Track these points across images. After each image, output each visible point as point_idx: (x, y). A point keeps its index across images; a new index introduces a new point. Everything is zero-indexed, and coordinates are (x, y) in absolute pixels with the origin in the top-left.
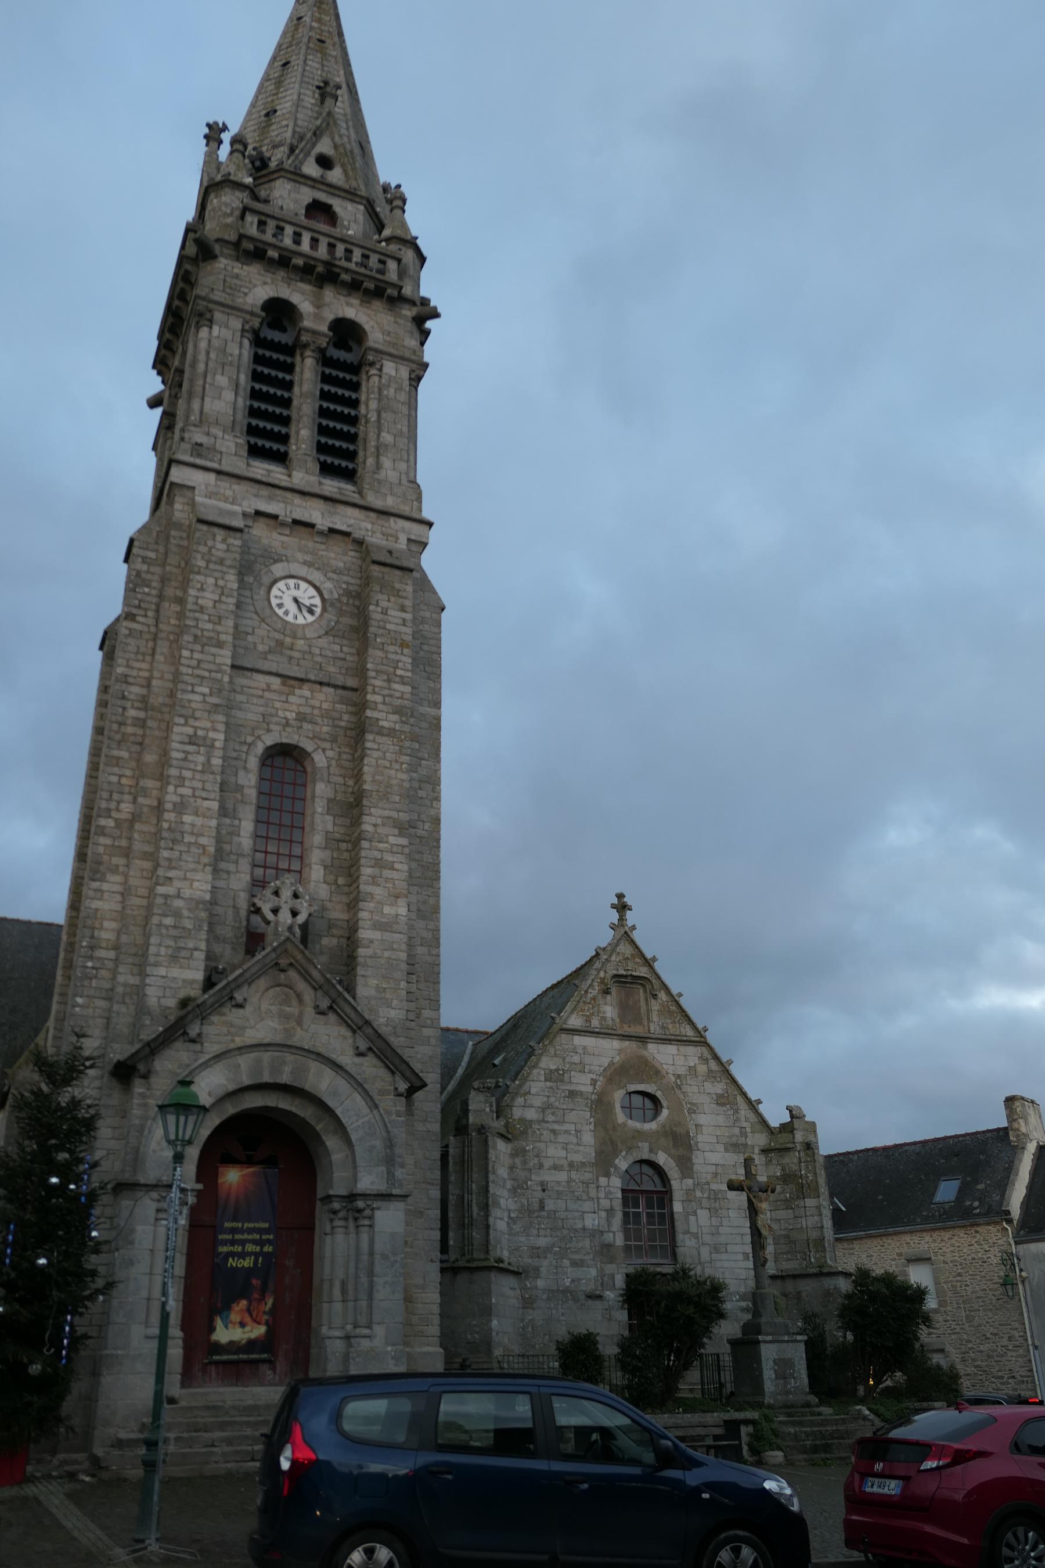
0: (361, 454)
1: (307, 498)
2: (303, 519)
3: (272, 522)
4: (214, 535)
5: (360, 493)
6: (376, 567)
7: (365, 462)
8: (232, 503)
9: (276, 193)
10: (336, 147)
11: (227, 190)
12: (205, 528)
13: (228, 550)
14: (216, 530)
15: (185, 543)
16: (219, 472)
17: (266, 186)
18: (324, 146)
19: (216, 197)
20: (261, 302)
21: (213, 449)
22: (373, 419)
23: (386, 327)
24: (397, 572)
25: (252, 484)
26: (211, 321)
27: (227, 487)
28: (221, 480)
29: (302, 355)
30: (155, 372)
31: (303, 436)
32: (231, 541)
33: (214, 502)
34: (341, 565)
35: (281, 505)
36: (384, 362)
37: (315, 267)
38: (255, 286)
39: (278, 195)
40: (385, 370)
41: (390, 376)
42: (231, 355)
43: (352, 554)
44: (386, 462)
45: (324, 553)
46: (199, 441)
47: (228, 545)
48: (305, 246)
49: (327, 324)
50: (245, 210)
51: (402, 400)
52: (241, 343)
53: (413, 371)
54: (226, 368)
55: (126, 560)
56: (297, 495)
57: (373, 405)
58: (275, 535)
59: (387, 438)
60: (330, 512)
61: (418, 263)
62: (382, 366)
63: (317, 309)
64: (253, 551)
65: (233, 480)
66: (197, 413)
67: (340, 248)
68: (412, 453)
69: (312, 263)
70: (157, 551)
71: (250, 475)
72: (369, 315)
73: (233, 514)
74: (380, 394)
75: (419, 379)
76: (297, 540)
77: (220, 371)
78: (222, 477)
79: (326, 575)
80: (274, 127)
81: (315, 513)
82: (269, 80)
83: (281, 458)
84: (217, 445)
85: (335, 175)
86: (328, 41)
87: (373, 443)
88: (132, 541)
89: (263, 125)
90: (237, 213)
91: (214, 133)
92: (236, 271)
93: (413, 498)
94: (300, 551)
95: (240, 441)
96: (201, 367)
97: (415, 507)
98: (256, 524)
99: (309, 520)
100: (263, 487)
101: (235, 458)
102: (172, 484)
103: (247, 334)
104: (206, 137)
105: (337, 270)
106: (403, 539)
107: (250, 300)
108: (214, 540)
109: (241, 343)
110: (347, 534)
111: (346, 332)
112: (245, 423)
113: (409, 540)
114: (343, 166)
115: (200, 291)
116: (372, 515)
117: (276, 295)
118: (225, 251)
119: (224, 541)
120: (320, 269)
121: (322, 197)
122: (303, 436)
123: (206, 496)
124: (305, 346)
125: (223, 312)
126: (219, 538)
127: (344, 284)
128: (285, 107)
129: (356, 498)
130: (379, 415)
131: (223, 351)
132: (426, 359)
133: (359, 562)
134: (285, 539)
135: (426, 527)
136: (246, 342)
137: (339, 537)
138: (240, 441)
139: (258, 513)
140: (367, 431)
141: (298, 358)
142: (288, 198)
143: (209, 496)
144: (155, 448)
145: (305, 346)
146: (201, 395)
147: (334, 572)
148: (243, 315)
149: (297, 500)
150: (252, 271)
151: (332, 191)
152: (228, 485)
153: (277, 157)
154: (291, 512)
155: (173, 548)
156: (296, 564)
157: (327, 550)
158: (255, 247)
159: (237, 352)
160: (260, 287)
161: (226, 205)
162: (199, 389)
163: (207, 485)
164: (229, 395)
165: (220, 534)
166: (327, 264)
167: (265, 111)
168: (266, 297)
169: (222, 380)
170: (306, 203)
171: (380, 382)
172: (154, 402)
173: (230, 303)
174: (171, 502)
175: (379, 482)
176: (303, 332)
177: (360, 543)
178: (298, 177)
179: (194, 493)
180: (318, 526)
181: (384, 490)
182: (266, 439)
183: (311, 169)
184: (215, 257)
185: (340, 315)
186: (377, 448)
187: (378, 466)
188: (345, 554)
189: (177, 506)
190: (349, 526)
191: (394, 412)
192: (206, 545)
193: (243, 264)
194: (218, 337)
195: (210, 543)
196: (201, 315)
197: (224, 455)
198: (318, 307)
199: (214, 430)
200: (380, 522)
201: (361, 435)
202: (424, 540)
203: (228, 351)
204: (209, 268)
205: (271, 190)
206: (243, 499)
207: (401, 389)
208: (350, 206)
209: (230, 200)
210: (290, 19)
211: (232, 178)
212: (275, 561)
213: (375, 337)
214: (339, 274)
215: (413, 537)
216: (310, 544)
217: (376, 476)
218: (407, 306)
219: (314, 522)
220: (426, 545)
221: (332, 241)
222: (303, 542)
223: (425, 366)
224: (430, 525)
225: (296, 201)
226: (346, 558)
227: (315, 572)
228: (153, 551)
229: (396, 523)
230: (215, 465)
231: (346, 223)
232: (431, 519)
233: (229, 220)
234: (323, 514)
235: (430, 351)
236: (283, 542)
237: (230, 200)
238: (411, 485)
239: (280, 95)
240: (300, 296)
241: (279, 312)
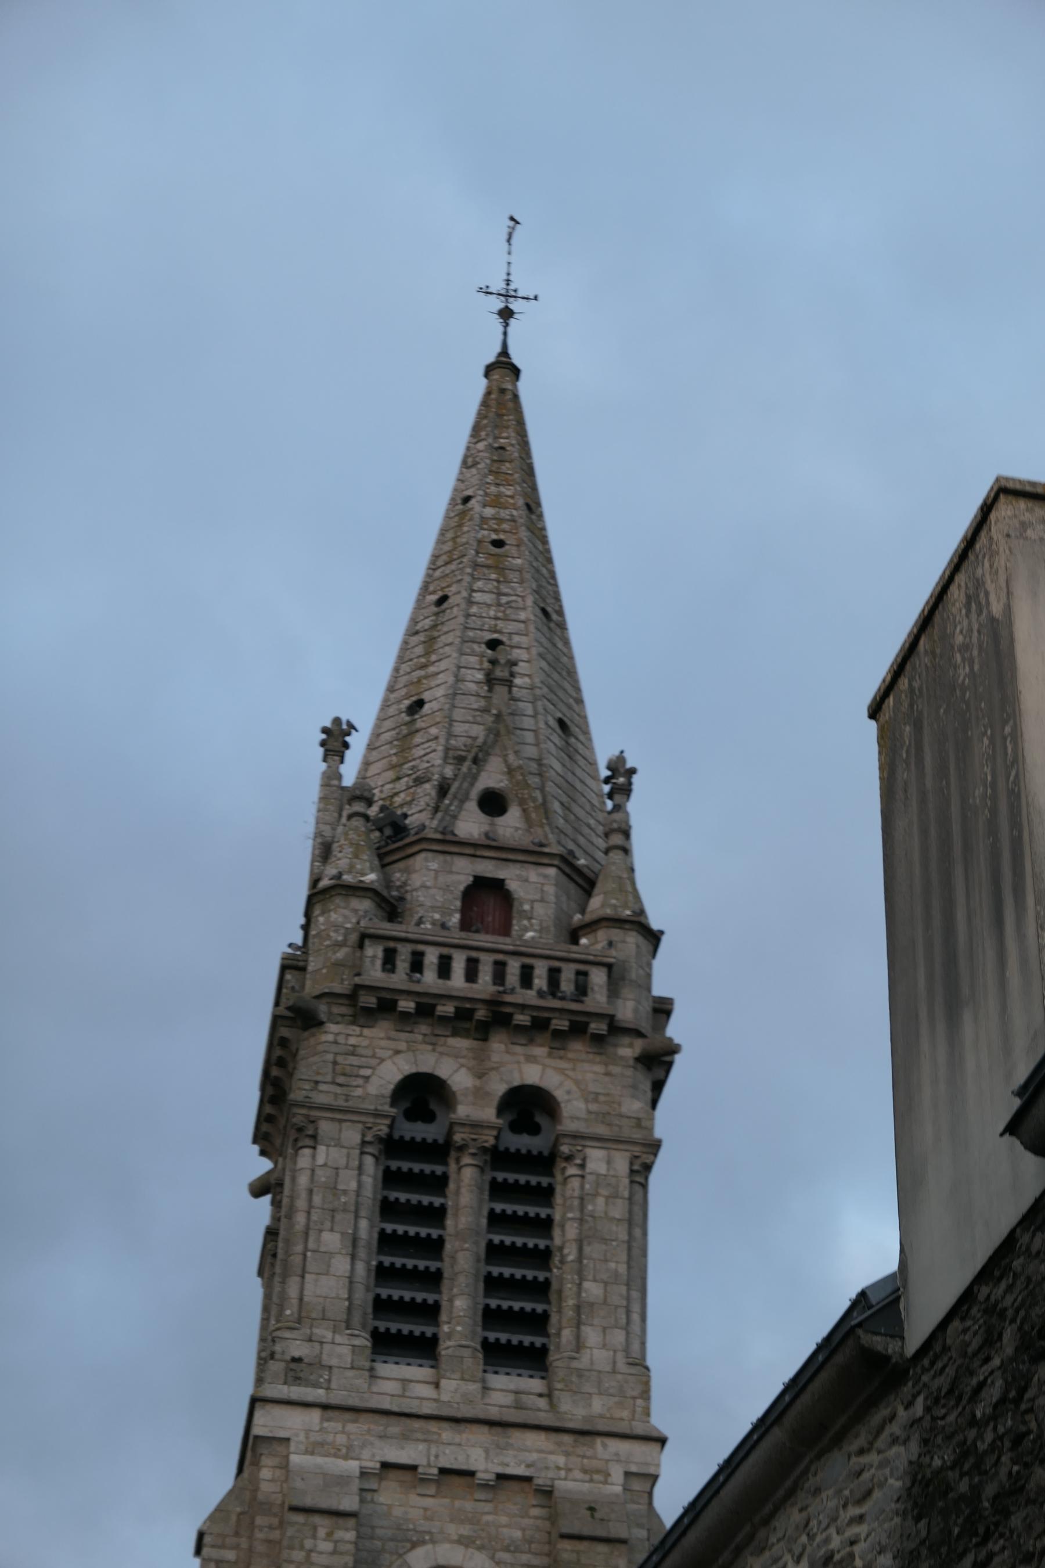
0: (554, 1319)
1: (462, 1427)
2: (455, 1466)
3: (407, 1476)
4: (315, 1528)
5: (548, 1395)
6: (567, 1545)
7: (558, 1334)
8: (346, 1458)
9: (416, 880)
10: (510, 771)
11: (338, 900)
12: (300, 1518)
13: (335, 1552)
14: (317, 1519)
15: (276, 1535)
16: (325, 1407)
17: (401, 865)
18: (493, 776)
19: (323, 913)
20: (392, 1087)
21: (318, 1364)
22: (571, 1258)
23: (592, 1088)
24: (602, 1548)
25: (377, 1417)
26: (314, 1137)
27: (339, 1430)
28: (328, 1420)
29: (458, 1160)
30: (256, 1148)
31: (460, 1307)
32: (340, 1534)
33: (319, 1460)
34: (518, 1534)
35: (421, 1447)
36: (589, 1152)
37: (472, 1011)
38: (382, 1060)
39: (418, 884)
40: (591, 1166)
41: (598, 1175)
42: (345, 1192)
43: (535, 1512)
44: (591, 1335)
45: (490, 1518)
46: (297, 1354)
47: (336, 1542)
48: (458, 980)
49: (495, 1102)
50: (364, 938)
51: (618, 1216)
52: (360, 1168)
53: (637, 1157)
54: (339, 1217)
55: (198, 1552)
56: (445, 1425)
57: (572, 1231)
58: (414, 1499)
59: (593, 1290)
60: (498, 1447)
61: (645, 945)
62: (584, 1159)
63: (476, 1080)
64: (379, 1532)
65: (348, 1416)
66: (295, 1302)
67: (514, 967)
68: (636, 1308)
69: (468, 1006)
70: (236, 1547)
71: (374, 1403)
72: (561, 1071)
73: (342, 1480)
74: (582, 1208)
75: (648, 1168)
76: (447, 1501)
77: (328, 1224)
78: (330, 1414)
79: (492, 1558)
80: (418, 739)
81: (476, 1452)
82: (417, 633)
83: (425, 1349)
84: (324, 1357)
85: (510, 825)
86: (510, 540)
87: (571, 1302)
88: (201, 1535)
89: (405, 730)
90: (354, 937)
91: (335, 740)
92: (352, 1041)
93: (635, 1393)
94: (452, 1521)
95: (357, 1342)
96: (300, 1219)
97: (639, 1410)
98: (384, 1484)
99: (464, 1467)
100: (393, 1420)
101: (350, 1373)
102: (256, 1437)
103: (369, 1149)
104: (323, 744)
105: (508, 1010)
106: (617, 1474)
107: (372, 1089)
108: (314, 1537)
109: (360, 1168)
110: (528, 1479)
111: (527, 1106)
112: (370, 1297)
113: (628, 1474)
114: (522, 802)
115: (296, 1095)
116: (567, 1439)
117: (414, 1070)
118: (336, 1010)
119: (330, 1535)
120: (481, 1014)
121: (488, 869)
122: (460, 1307)
123: (307, 1452)
124: (461, 1149)
125: (332, 1119)
126: (322, 1532)
127: (520, 1029)
128: (436, 697)
129: (540, 1411)
130: (580, 1250)
131: (333, 1188)
132: (658, 1133)
133: (547, 1524)
134: (429, 1502)
135: (656, 1446)
136: (369, 1161)
137: (514, 1485)
138: (357, 1342)
139: (386, 1466)
140: (562, 1275)
141: (453, 1166)
142: (434, 886)
143: (311, 1450)
144: (260, 1273)
145: (461, 1149)
146: (299, 1272)
147: (507, 1549)
148: (363, 1119)
149: (447, 1433)
150: (378, 1036)
151: (504, 855)
152: (339, 1426)
153: (417, 817)
154: (437, 1456)
155: (260, 1548)
156: (447, 1546)
157: (495, 1513)
158: (379, 999)
159: (353, 1185)
160: (388, 1060)
161: (337, 927)
162: (297, 1260)
163: (308, 1432)
164: (341, 1265)
165: (323, 1524)
166: (493, 1004)
167: (408, 706)
168: (399, 1077)
169: (331, 1240)
170: (462, 888)
171: (582, 1187)
172: (259, 1189)
173: (341, 1102)
174: (256, 1463)
175: (580, 1373)
176: (456, 1128)
177: (547, 1493)
178: (449, 844)
179: (288, 1447)
180: (479, 1475)
181: (588, 1388)
182: (401, 1327)
183: (471, 824)
184: (321, 1023)
185: (516, 1083)
186: (578, 1308)
187: (579, 1345)
188: (525, 1515)
189: (265, 1474)
190: (528, 1466)
191: (605, 1241)
192: (302, 1547)
193: (362, 1026)
194: (325, 1165)
195: (308, 1543)
196: (300, 1130)
197: (335, 1371)
198: (480, 1076)
199: (323, 1332)
200: (580, 1451)
201: (555, 1286)
202: (652, 1470)
203: (341, 1187)
204: (312, 1041)
205: (408, 871)
206: (363, 1446)
207: (615, 1196)
208: (533, 874)
209: (346, 916)
210: (453, 502)
211: (347, 878)
212: (414, 1545)
213: (574, 1110)
214: (511, 1015)
215: (634, 1469)
216: (469, 1506)
217: (575, 1364)
218: (626, 1040)
219: (473, 1468)
220: (655, 1478)
221: (500, 957)
222: (458, 1504)
223: (655, 1146)
224: (662, 1441)
225: (446, 889)
226: (527, 1522)
227: (477, 1553)
228: (232, 1548)
229: (604, 1446)
230: (318, 1394)
231: (527, 907)
232: (665, 1429)
233: (341, 954)
234: (487, 1451)
235: (665, 1121)
236: (426, 1509)
237: (346, 916)
238: (633, 1370)
239: (432, 669)
240: (452, 1064)
241: (421, 1094)
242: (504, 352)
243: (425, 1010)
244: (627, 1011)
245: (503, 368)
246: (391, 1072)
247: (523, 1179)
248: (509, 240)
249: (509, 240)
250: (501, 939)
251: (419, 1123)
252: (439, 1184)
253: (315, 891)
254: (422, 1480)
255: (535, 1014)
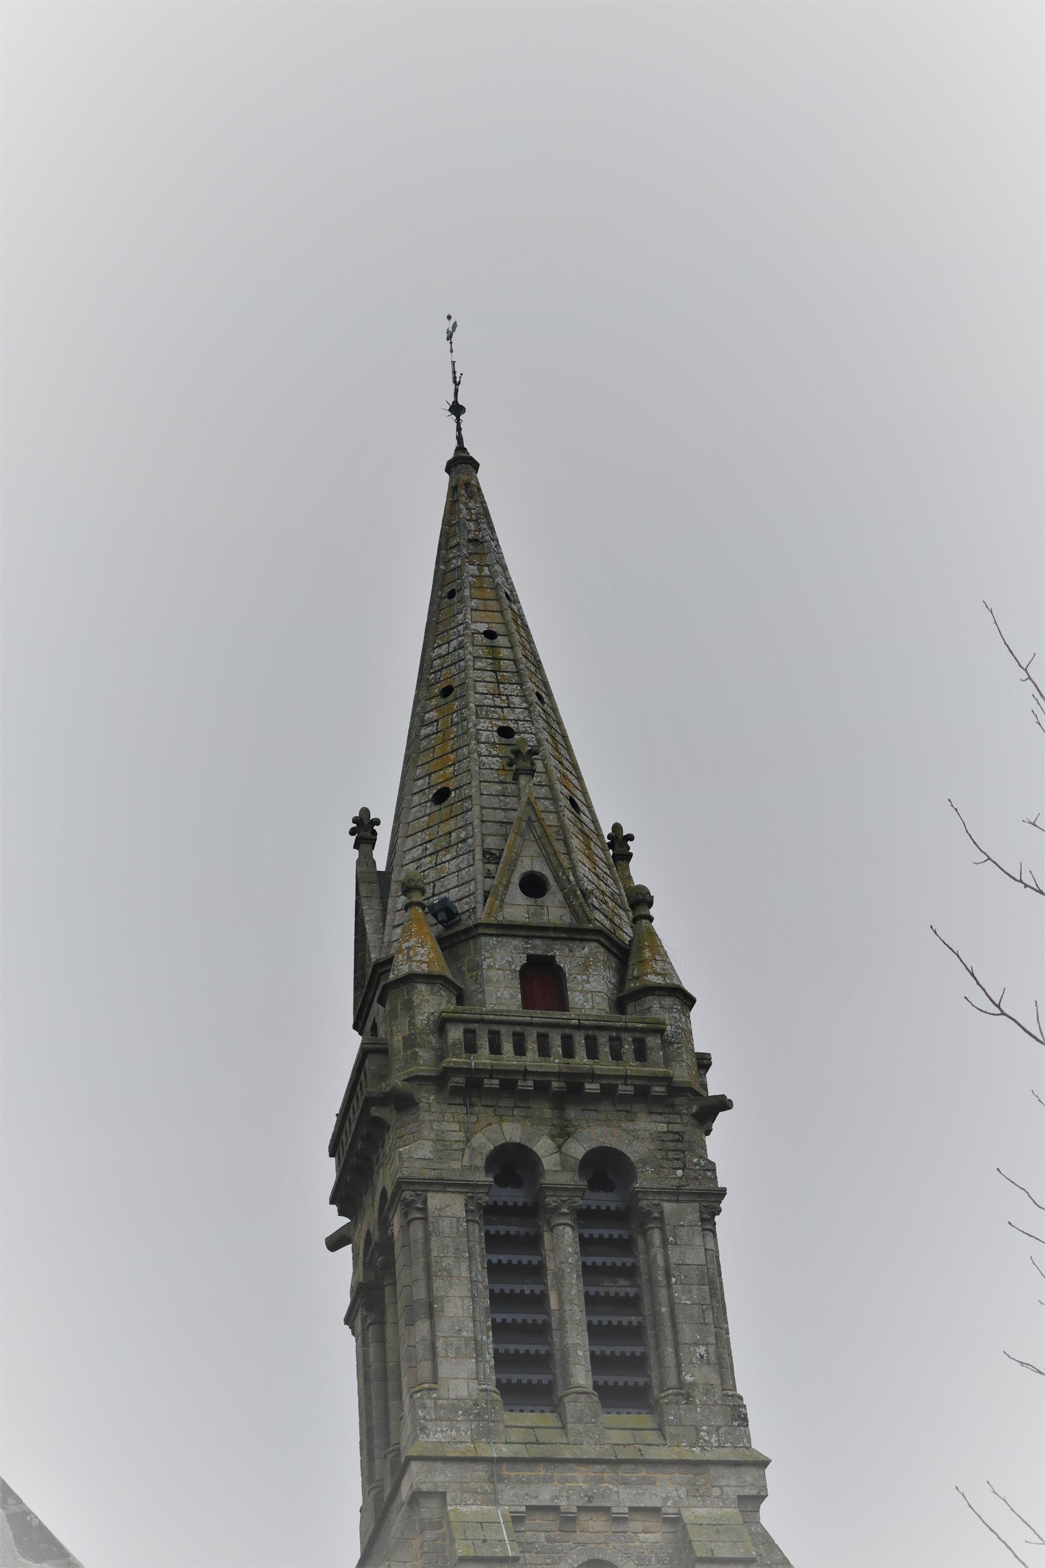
111: (604, 1168)
145: (555, 1210)
182: (524, 1374)
183: (518, 908)
241: (512, 1164)
242: (461, 448)
243: (542, 1087)
244: (682, 1073)
245: (462, 465)
246: (485, 1141)
247: (606, 1233)
248: (449, 337)
249: (449, 337)
250: (556, 1014)
251: (509, 1188)
252: (534, 1243)
253: (625, 993)
254: (614, 1519)
255: (605, 1082)
